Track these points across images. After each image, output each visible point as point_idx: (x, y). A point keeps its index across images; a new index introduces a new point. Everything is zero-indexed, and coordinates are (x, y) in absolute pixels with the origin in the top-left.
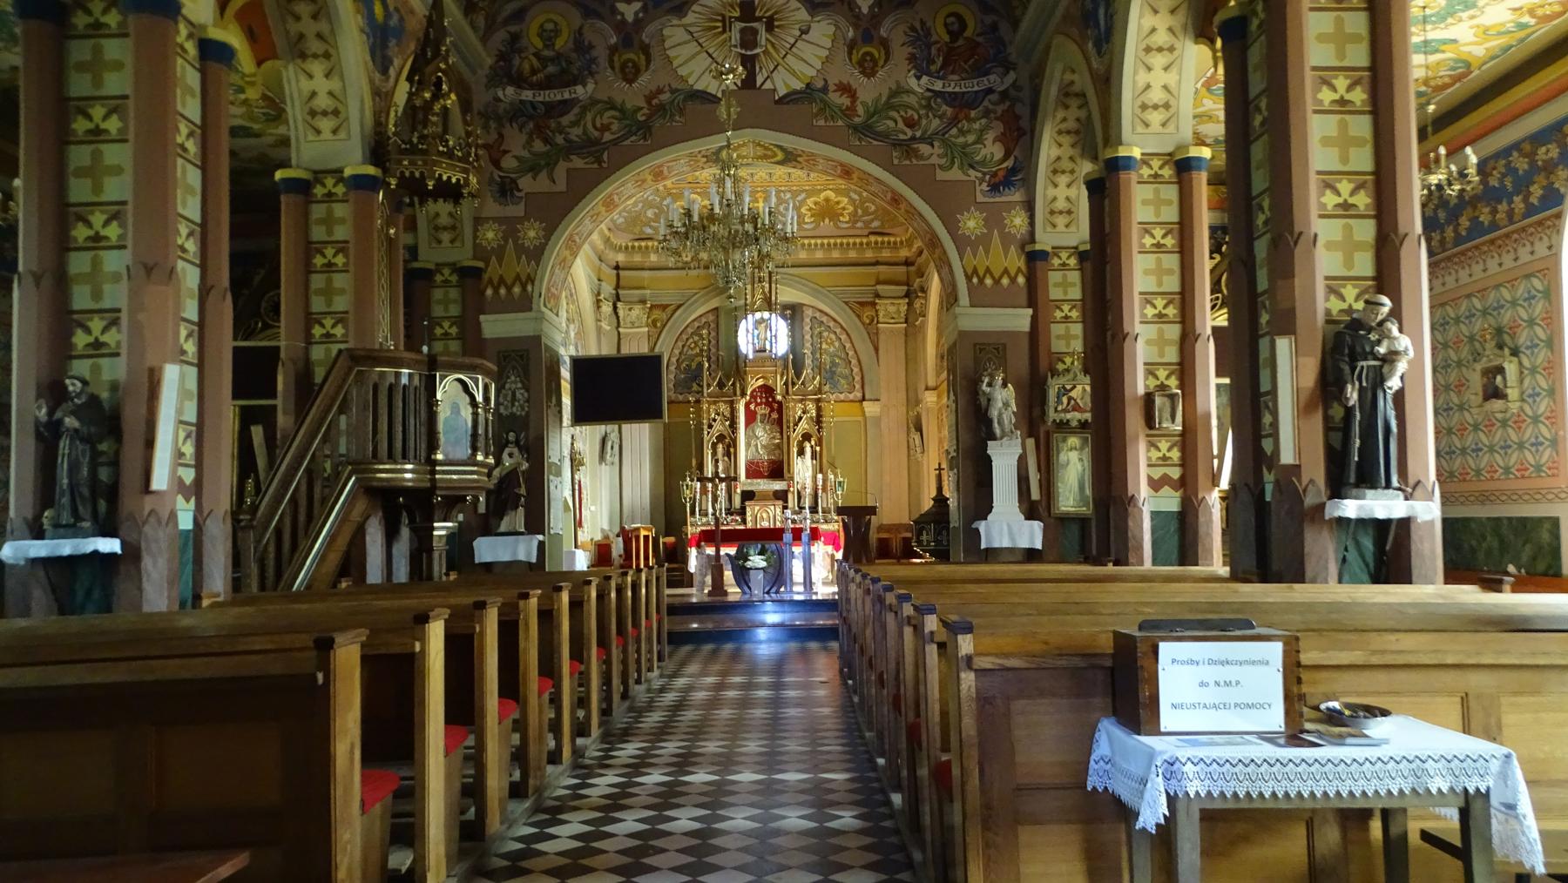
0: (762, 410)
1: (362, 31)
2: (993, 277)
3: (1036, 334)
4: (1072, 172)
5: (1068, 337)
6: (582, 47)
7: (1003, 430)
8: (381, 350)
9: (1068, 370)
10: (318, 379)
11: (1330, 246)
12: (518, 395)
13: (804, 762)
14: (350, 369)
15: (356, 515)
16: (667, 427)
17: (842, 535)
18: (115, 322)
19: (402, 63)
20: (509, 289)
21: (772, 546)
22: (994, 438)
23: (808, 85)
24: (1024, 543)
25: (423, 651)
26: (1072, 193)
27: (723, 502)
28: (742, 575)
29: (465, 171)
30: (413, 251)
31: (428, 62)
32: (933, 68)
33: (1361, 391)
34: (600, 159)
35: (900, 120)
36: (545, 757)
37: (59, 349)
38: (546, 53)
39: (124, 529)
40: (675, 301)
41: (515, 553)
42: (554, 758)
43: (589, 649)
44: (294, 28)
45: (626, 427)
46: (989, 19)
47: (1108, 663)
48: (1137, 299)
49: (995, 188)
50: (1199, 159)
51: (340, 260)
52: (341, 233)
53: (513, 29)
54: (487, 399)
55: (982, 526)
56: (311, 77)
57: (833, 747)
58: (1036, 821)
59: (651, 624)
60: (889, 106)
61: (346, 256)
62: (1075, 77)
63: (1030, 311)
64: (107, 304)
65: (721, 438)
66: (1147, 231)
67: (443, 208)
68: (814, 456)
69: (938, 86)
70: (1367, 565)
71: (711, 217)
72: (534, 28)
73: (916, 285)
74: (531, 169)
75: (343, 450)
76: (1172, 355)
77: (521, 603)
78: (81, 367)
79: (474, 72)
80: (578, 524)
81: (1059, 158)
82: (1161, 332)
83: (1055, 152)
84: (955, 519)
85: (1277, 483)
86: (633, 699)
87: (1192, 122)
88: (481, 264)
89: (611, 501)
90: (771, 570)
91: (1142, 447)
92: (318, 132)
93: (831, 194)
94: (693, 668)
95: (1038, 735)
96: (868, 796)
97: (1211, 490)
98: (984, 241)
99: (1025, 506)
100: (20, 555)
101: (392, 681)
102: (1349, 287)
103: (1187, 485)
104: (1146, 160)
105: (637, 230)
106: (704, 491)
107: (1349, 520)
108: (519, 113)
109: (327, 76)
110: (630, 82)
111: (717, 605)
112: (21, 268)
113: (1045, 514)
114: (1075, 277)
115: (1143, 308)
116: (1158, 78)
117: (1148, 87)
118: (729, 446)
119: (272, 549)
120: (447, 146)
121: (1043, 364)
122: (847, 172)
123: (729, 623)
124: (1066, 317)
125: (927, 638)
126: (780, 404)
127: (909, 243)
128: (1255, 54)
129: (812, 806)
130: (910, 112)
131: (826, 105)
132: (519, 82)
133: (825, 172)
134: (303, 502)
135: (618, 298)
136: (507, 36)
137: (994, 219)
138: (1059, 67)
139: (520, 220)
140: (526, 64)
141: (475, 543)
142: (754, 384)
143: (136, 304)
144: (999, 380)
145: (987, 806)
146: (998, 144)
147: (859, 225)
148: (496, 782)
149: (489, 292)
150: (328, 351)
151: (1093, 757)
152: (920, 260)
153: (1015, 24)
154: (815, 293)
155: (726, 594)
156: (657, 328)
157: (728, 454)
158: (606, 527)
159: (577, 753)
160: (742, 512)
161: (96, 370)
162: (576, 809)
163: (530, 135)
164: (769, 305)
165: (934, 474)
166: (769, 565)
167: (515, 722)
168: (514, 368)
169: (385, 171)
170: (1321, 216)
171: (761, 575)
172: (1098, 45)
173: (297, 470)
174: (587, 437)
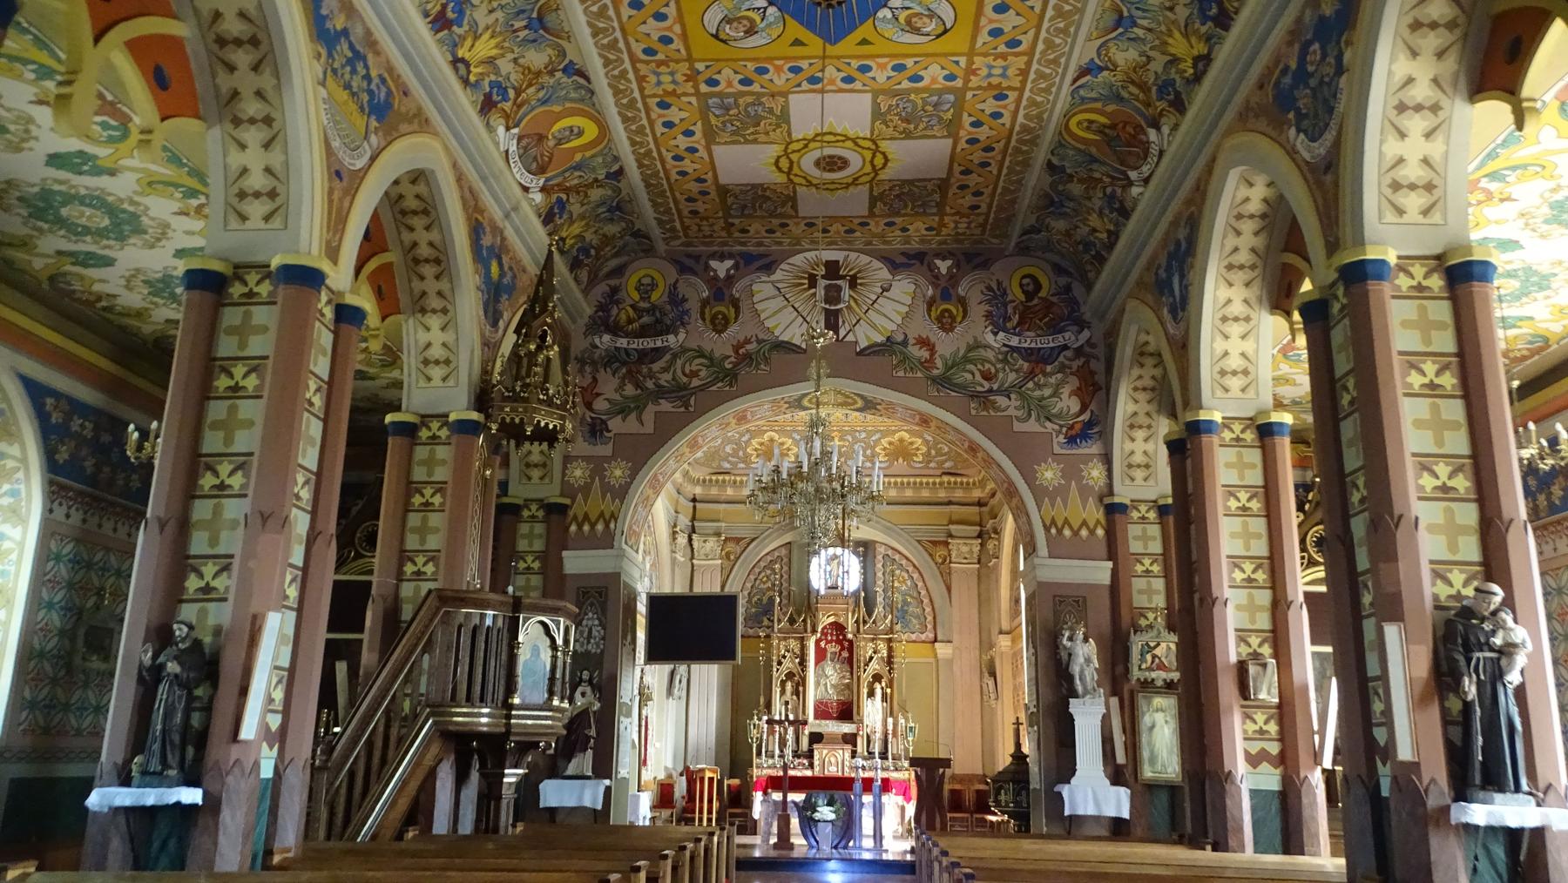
0: (832, 648)
2: (1071, 528)
3: (1116, 589)
4: (1149, 427)
5: (1150, 592)
6: (676, 300)
7: (1085, 688)
8: (467, 591)
9: (1151, 627)
11: (1431, 529)
12: (595, 633)
14: (438, 609)
15: (428, 761)
16: (735, 668)
17: (913, 784)
18: (226, 568)
19: (512, 317)
20: (593, 526)
21: (838, 794)
22: (1076, 696)
24: (1110, 812)
26: (1150, 447)
27: (788, 752)
28: (809, 825)
29: (562, 418)
30: (504, 486)
31: (536, 317)
33: (1479, 684)
34: (689, 402)
37: (173, 595)
38: (643, 305)
39: (207, 779)
40: (748, 534)
41: (580, 798)
44: (417, 286)
45: (695, 667)
46: (1063, 281)
48: (1224, 562)
49: (1071, 441)
50: (1281, 424)
51: (437, 500)
52: (440, 474)
53: (613, 282)
54: (566, 642)
55: (1065, 790)
56: (428, 329)
60: (966, 360)
61: (443, 496)
63: (1110, 564)
64: (220, 550)
65: (790, 675)
66: (1232, 494)
67: (536, 450)
68: (884, 698)
69: (1014, 341)
70: (1500, 876)
72: (633, 280)
75: (423, 690)
76: (1264, 621)
78: (188, 612)
79: (574, 322)
80: (643, 762)
83: (1131, 407)
84: (1035, 782)
85: (1395, 779)
87: (1271, 383)
88: (567, 501)
91: (1237, 718)
92: (429, 379)
93: (906, 435)
97: (1313, 769)
98: (1061, 492)
99: (1110, 769)
100: (106, 803)
102: (1456, 572)
103: (1286, 760)
104: (1227, 423)
107: (1477, 827)
108: (613, 359)
110: (719, 332)
112: (148, 515)
113: (1131, 780)
114: (1155, 530)
117: (1226, 354)
118: (798, 684)
119: (343, 791)
122: (925, 421)
124: (1147, 571)
126: (851, 642)
127: (982, 484)
128: (1339, 335)
130: (987, 366)
131: (906, 358)
132: (615, 330)
134: (379, 743)
137: (1072, 472)
138: (1133, 329)
139: (608, 459)
140: (623, 314)
141: (541, 786)
142: (825, 621)
143: (248, 554)
144: (1080, 634)
149: (573, 528)
150: (417, 589)
152: (993, 502)
153: (1089, 287)
154: (887, 531)
155: (791, 847)
156: (730, 560)
157: (796, 693)
158: (670, 765)
161: (203, 614)
163: (623, 379)
164: (842, 541)
168: (592, 605)
169: (488, 417)
170: (1420, 498)
171: (830, 826)
172: (1173, 312)
173: (376, 710)
174: (656, 675)
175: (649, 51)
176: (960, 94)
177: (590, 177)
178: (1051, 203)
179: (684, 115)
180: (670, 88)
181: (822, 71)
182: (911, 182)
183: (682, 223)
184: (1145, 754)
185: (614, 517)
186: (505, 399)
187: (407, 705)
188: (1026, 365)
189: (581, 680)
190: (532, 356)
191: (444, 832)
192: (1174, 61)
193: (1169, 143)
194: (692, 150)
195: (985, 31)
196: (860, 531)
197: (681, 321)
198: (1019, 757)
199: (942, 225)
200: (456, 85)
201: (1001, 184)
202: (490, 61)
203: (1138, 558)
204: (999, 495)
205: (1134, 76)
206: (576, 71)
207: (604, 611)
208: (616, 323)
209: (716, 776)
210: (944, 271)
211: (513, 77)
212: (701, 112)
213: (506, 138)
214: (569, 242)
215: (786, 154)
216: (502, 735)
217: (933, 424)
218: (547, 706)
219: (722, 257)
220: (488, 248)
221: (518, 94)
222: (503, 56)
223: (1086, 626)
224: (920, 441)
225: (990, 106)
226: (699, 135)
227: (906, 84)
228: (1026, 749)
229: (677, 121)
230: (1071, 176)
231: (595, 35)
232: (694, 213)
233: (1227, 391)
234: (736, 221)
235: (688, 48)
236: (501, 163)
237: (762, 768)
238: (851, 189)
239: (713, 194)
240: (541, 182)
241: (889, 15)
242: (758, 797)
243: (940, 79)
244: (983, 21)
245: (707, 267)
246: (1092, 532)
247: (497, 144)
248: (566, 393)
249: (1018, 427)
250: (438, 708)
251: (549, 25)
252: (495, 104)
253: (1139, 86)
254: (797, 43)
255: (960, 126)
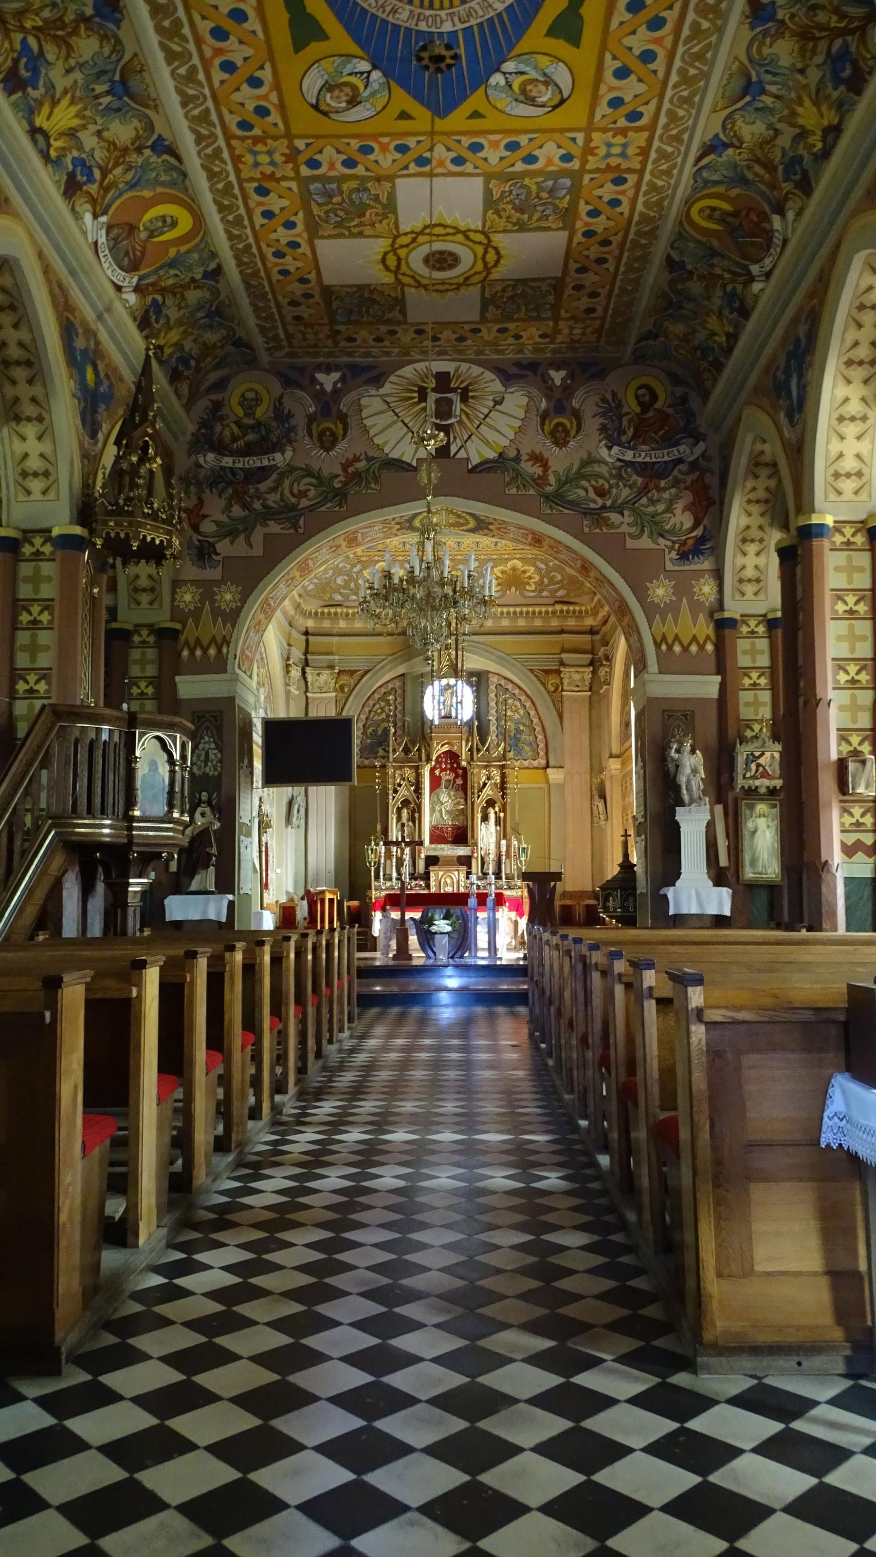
0: (446, 776)
1: (74, 395)
2: (681, 644)
3: (724, 702)
4: (761, 540)
5: (756, 704)
6: (281, 415)
9: (756, 737)
10: (21, 734)
13: (501, 1122)
16: (352, 789)
19: (110, 428)
20: (205, 651)
21: (456, 910)
22: (682, 804)
23: (501, 455)
24: (712, 910)
25: (139, 997)
26: (761, 561)
27: (406, 870)
28: (427, 939)
29: (169, 533)
30: (113, 612)
31: (136, 427)
32: (624, 439)
34: (297, 524)
35: (591, 490)
36: (246, 1111)
40: (363, 667)
41: (205, 911)
42: (255, 1113)
43: (287, 1005)
45: (313, 790)
46: (679, 391)
47: (842, 1018)
48: (830, 664)
49: (684, 556)
51: (45, 617)
52: (47, 591)
53: (215, 397)
54: (183, 757)
55: (670, 892)
56: (24, 439)
57: (531, 1109)
58: (767, 1178)
59: (342, 985)
60: (580, 476)
61: (51, 614)
62: (766, 447)
63: (718, 678)
65: (406, 803)
67: (144, 570)
68: (498, 822)
69: (629, 456)
71: (412, 579)
72: (235, 400)
73: (600, 654)
74: (229, 534)
75: (43, 805)
77: (227, 955)
79: (176, 438)
80: (265, 886)
81: (748, 527)
82: (853, 698)
83: (744, 521)
84: (642, 885)
86: (327, 1057)
88: (178, 626)
89: (296, 865)
90: (455, 935)
91: (835, 813)
92: (29, 492)
93: (518, 564)
94: (380, 1030)
95: (769, 1092)
96: (573, 1156)
98: (673, 608)
99: (713, 872)
101: (112, 1023)
105: (327, 597)
106: (388, 855)
108: (219, 479)
109: (39, 438)
110: (327, 450)
111: (402, 969)
114: (763, 644)
115: (836, 674)
116: (850, 447)
117: (841, 455)
118: (413, 811)
120: (152, 508)
121: (732, 732)
122: (537, 540)
123: (413, 985)
124: (755, 684)
125: (646, 993)
126: (465, 770)
127: (595, 614)
129: (516, 1167)
130: (601, 482)
132: (220, 448)
133: (514, 540)
135: (307, 664)
136: (210, 404)
138: (749, 438)
140: (227, 431)
141: (166, 901)
142: (439, 749)
144: (688, 746)
145: (718, 1162)
146: (687, 514)
147: (545, 594)
148: (203, 1135)
149: (185, 653)
150: (31, 707)
151: (826, 1114)
153: (705, 396)
154: (501, 661)
155: (410, 958)
156: (344, 693)
157: (412, 819)
158: (291, 890)
159: (276, 1109)
160: (426, 877)
162: (278, 1164)
163: (230, 499)
164: (455, 671)
165: (619, 840)
166: (454, 931)
167: (220, 1077)
168: (207, 728)
169: (92, 532)
171: (446, 938)
172: (790, 416)
175: (245, 125)
176: (576, 176)
177: (186, 277)
178: (671, 303)
179: (285, 203)
180: (268, 170)
181: (431, 150)
182: (524, 282)
183: (286, 331)
184: (747, 858)
185: (226, 641)
186: (111, 513)
187: (28, 820)
188: (640, 480)
189: (200, 801)
190: (134, 471)
191: (74, 935)
192: (803, 134)
193: (794, 230)
194: (294, 245)
195: (604, 102)
196: (473, 662)
197: (286, 439)
198: (627, 866)
199: (557, 331)
200: (36, 161)
201: (618, 284)
202: (71, 134)
203: (746, 671)
204: (613, 619)
205: (759, 153)
206: (166, 148)
207: (220, 735)
208: (221, 441)
209: (336, 898)
210: (558, 382)
211: (98, 154)
212: (302, 199)
213: (94, 228)
214: (168, 351)
215: (394, 250)
216: (124, 845)
217: (545, 544)
218: (167, 818)
219: (328, 369)
220: (82, 355)
221: (104, 176)
222: (84, 127)
223: (693, 738)
224: (532, 569)
225: (608, 191)
226: (300, 227)
227: (520, 167)
228: (634, 859)
229: (277, 211)
230: (691, 273)
231: (184, 105)
232: (298, 318)
233: (840, 493)
234: (342, 328)
235: (286, 123)
236: (90, 255)
237: (378, 891)
238: (462, 290)
239: (317, 298)
240: (135, 280)
241: (502, 82)
242: (378, 916)
243: (556, 160)
244: (603, 89)
245: (313, 380)
246: (702, 648)
247: (85, 233)
248: (171, 507)
249: (630, 543)
250: (59, 820)
251: (131, 83)
252: (79, 186)
253: (764, 166)
254: (404, 115)
255: (576, 216)
